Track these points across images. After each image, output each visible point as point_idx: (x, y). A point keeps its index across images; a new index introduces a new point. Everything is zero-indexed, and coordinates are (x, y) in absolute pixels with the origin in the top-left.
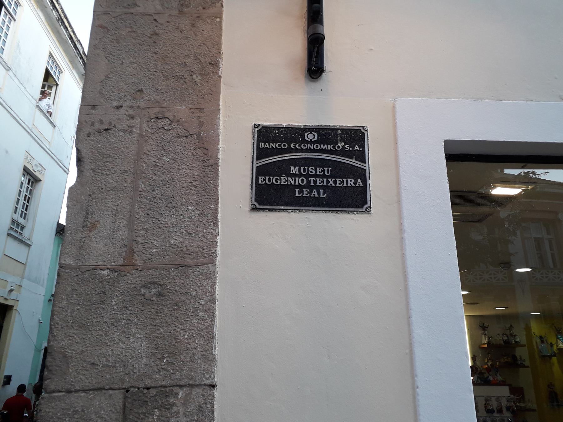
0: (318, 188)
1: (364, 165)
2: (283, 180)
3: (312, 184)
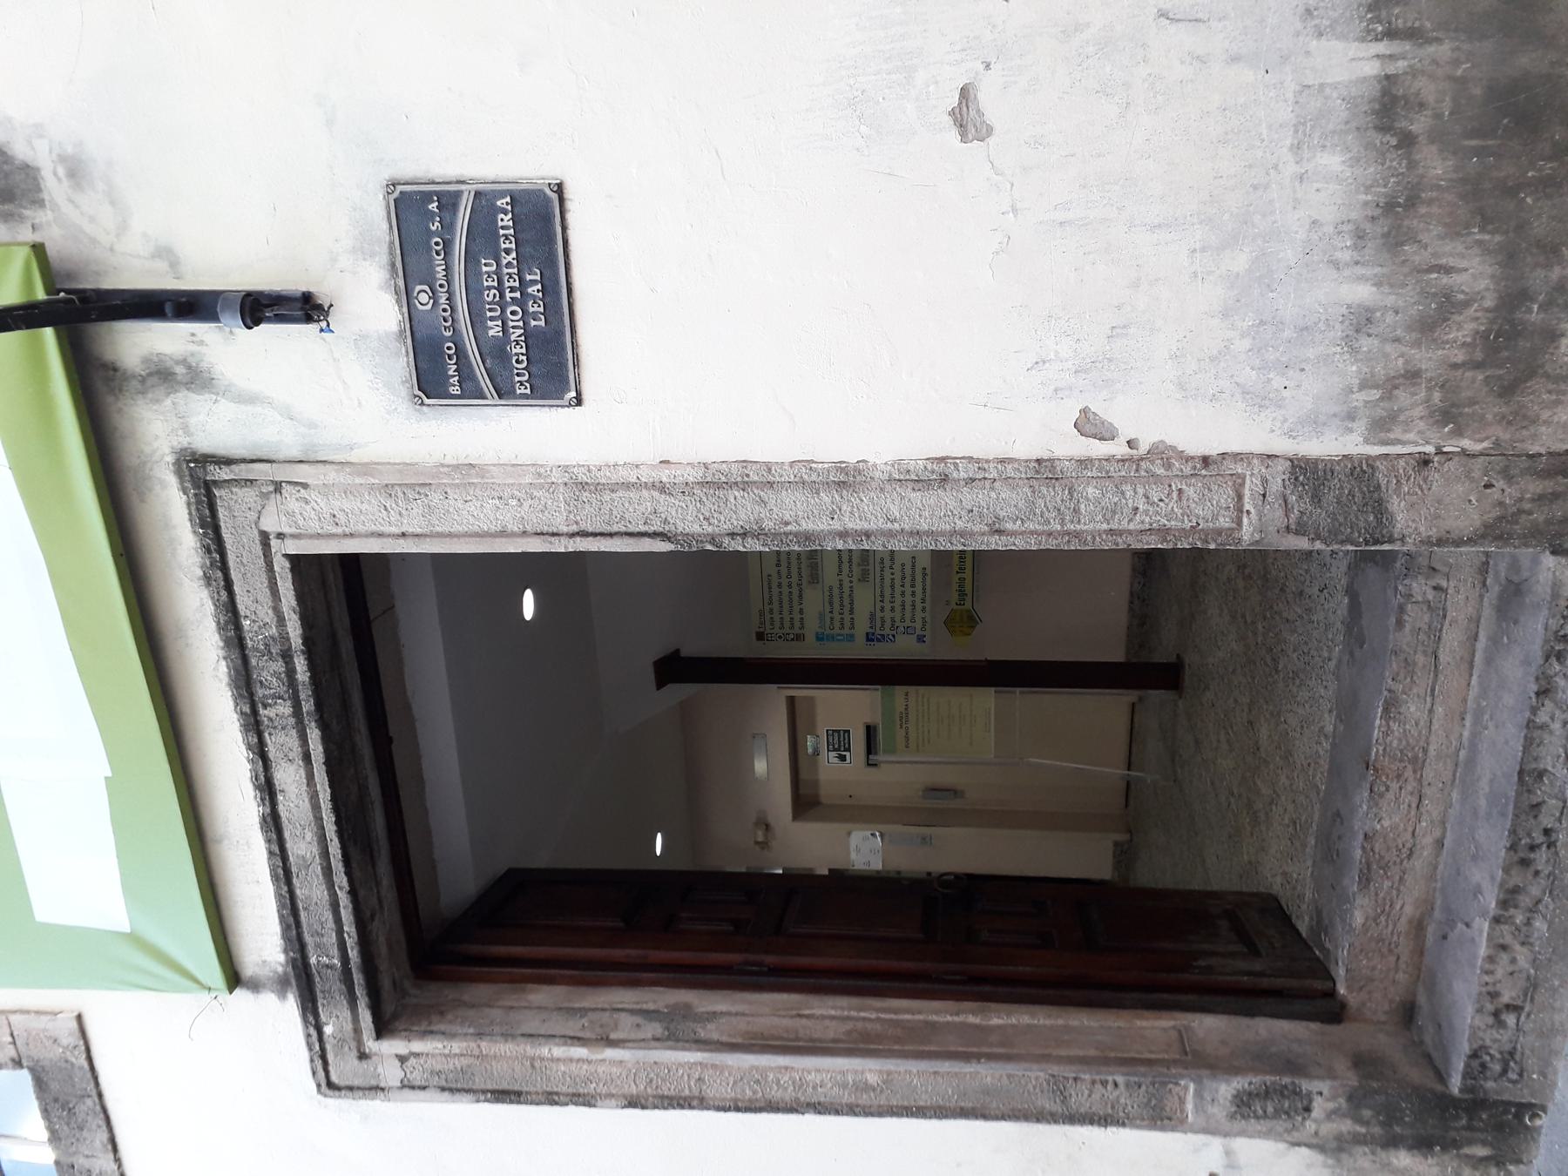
0: (523, 284)
1: (465, 195)
2: (518, 350)
3: (518, 295)
